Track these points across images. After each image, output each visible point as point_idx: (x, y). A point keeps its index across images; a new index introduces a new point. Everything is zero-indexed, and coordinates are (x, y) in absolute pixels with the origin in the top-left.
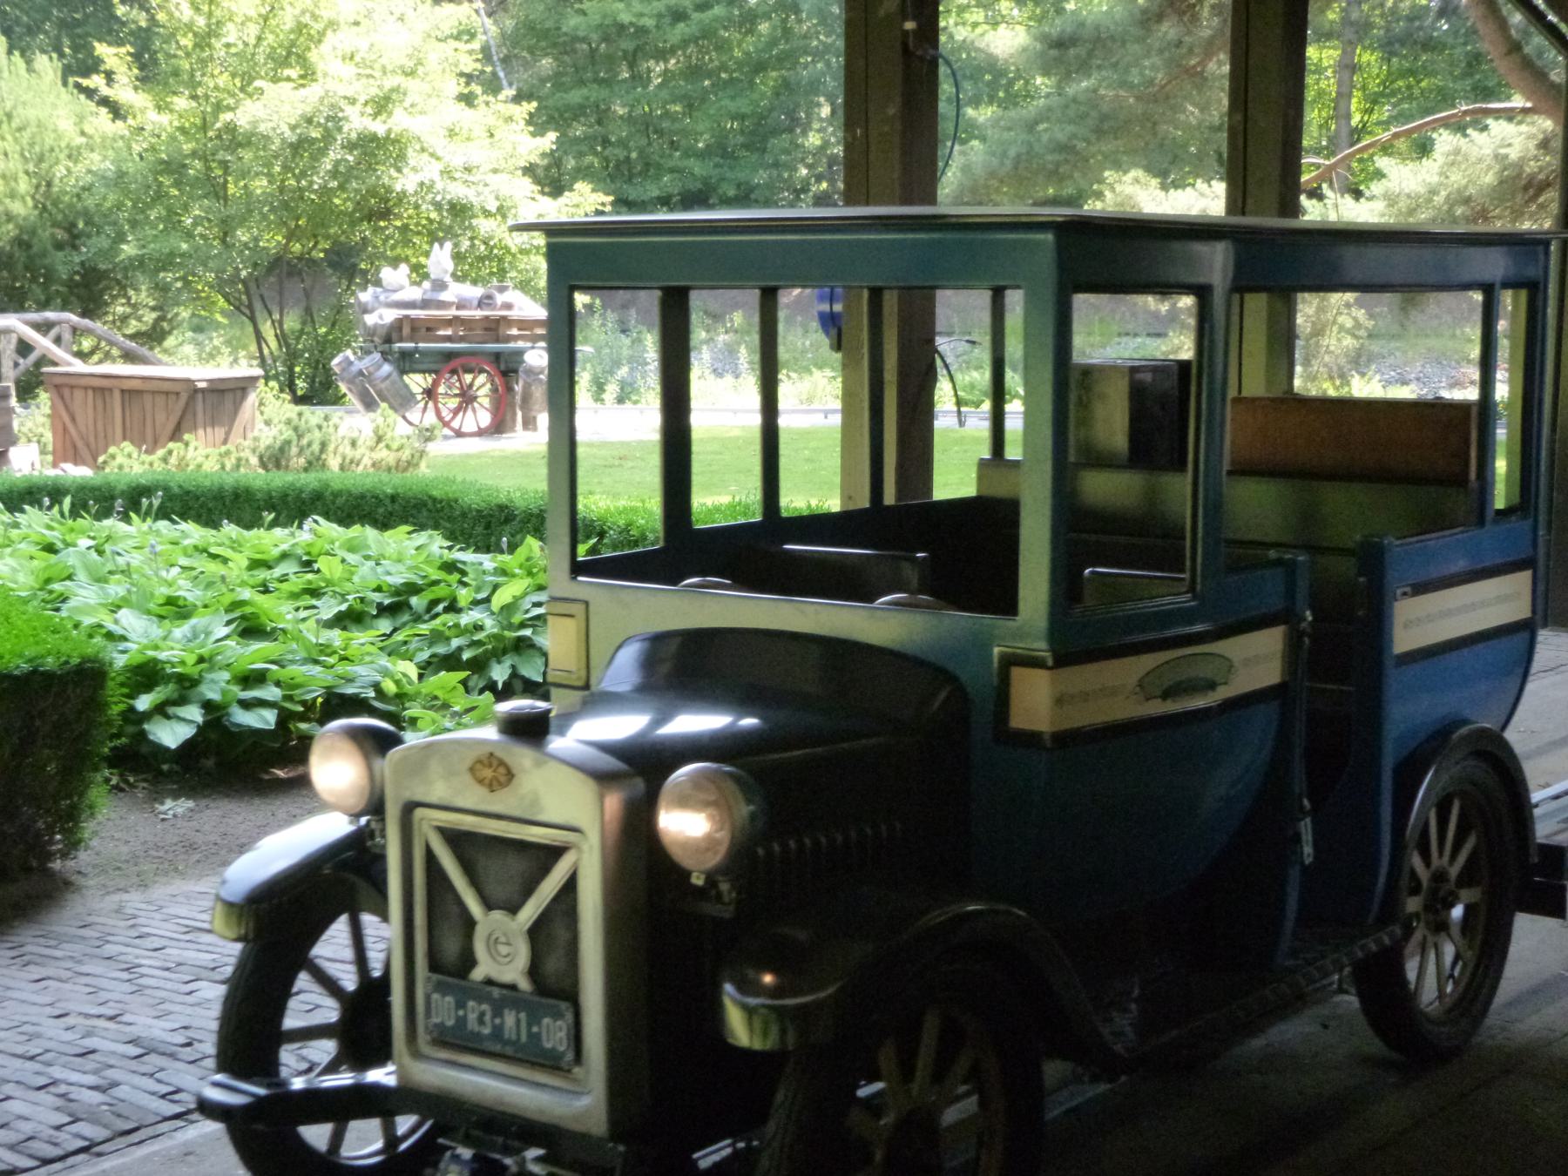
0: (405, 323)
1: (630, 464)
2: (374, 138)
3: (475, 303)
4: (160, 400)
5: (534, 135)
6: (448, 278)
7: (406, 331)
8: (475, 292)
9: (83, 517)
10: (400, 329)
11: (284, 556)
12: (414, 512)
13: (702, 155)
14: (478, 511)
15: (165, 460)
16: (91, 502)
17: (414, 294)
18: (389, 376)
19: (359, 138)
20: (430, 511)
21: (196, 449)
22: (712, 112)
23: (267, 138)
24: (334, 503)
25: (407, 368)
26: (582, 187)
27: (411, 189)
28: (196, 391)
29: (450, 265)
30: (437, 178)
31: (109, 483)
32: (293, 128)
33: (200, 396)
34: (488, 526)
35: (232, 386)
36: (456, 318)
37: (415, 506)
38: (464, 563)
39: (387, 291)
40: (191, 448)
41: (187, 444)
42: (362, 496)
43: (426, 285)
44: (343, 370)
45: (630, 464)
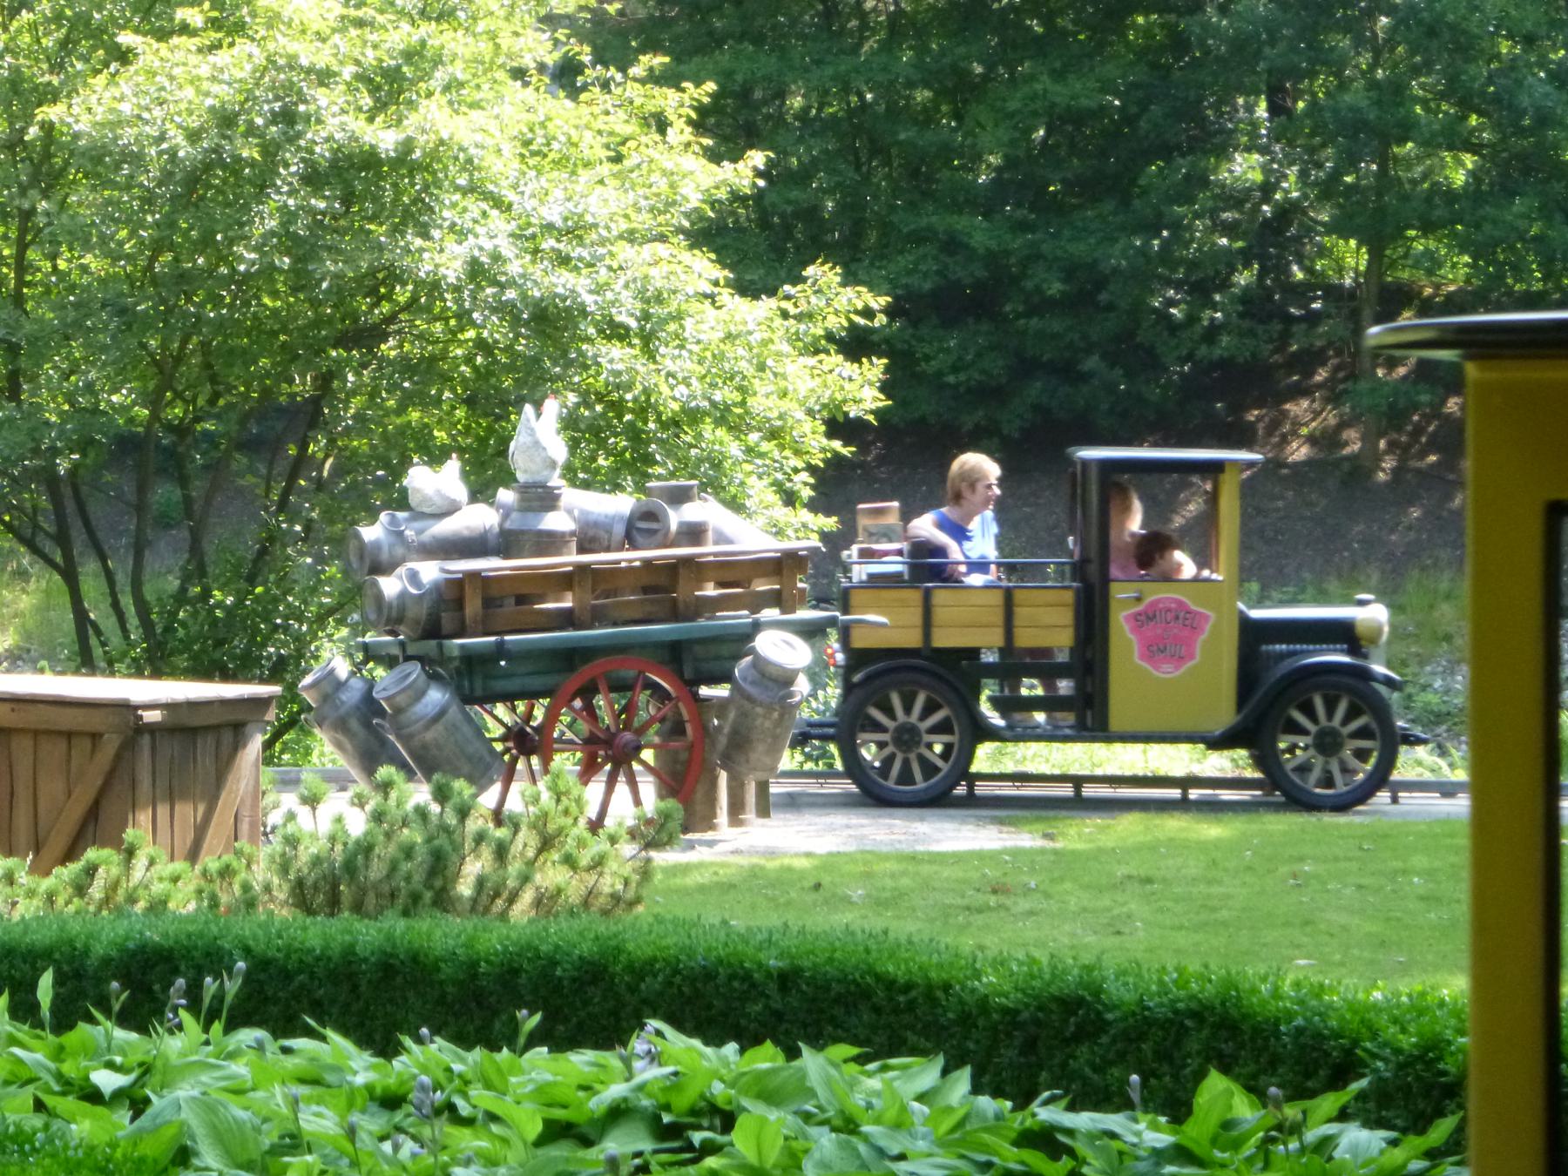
0: (468, 590)
1: (1024, 904)
2: (370, 161)
3: (619, 530)
4: (53, 751)
5: (714, 157)
6: (556, 481)
7: (473, 607)
8: (619, 505)
9: (91, 1020)
10: (459, 603)
11: (618, 1113)
12: (838, 1011)
13: (988, 203)
14: (1005, 1011)
15: (80, 890)
16: (115, 985)
17: (479, 518)
18: (442, 713)
19: (334, 163)
20: (877, 1010)
21: (152, 863)
22: (1013, 105)
23: (136, 159)
24: (633, 989)
25: (479, 692)
26: (822, 273)
27: (453, 271)
28: (142, 729)
29: (558, 449)
30: (507, 250)
31: (71, 942)
32: (193, 136)
33: (146, 740)
34: (1030, 1046)
35: (213, 720)
36: (582, 569)
37: (838, 1000)
38: (1070, 1132)
39: (420, 516)
40: (140, 862)
41: (130, 853)
42: (708, 975)
43: (506, 496)
44: (325, 698)
45: (1024, 904)
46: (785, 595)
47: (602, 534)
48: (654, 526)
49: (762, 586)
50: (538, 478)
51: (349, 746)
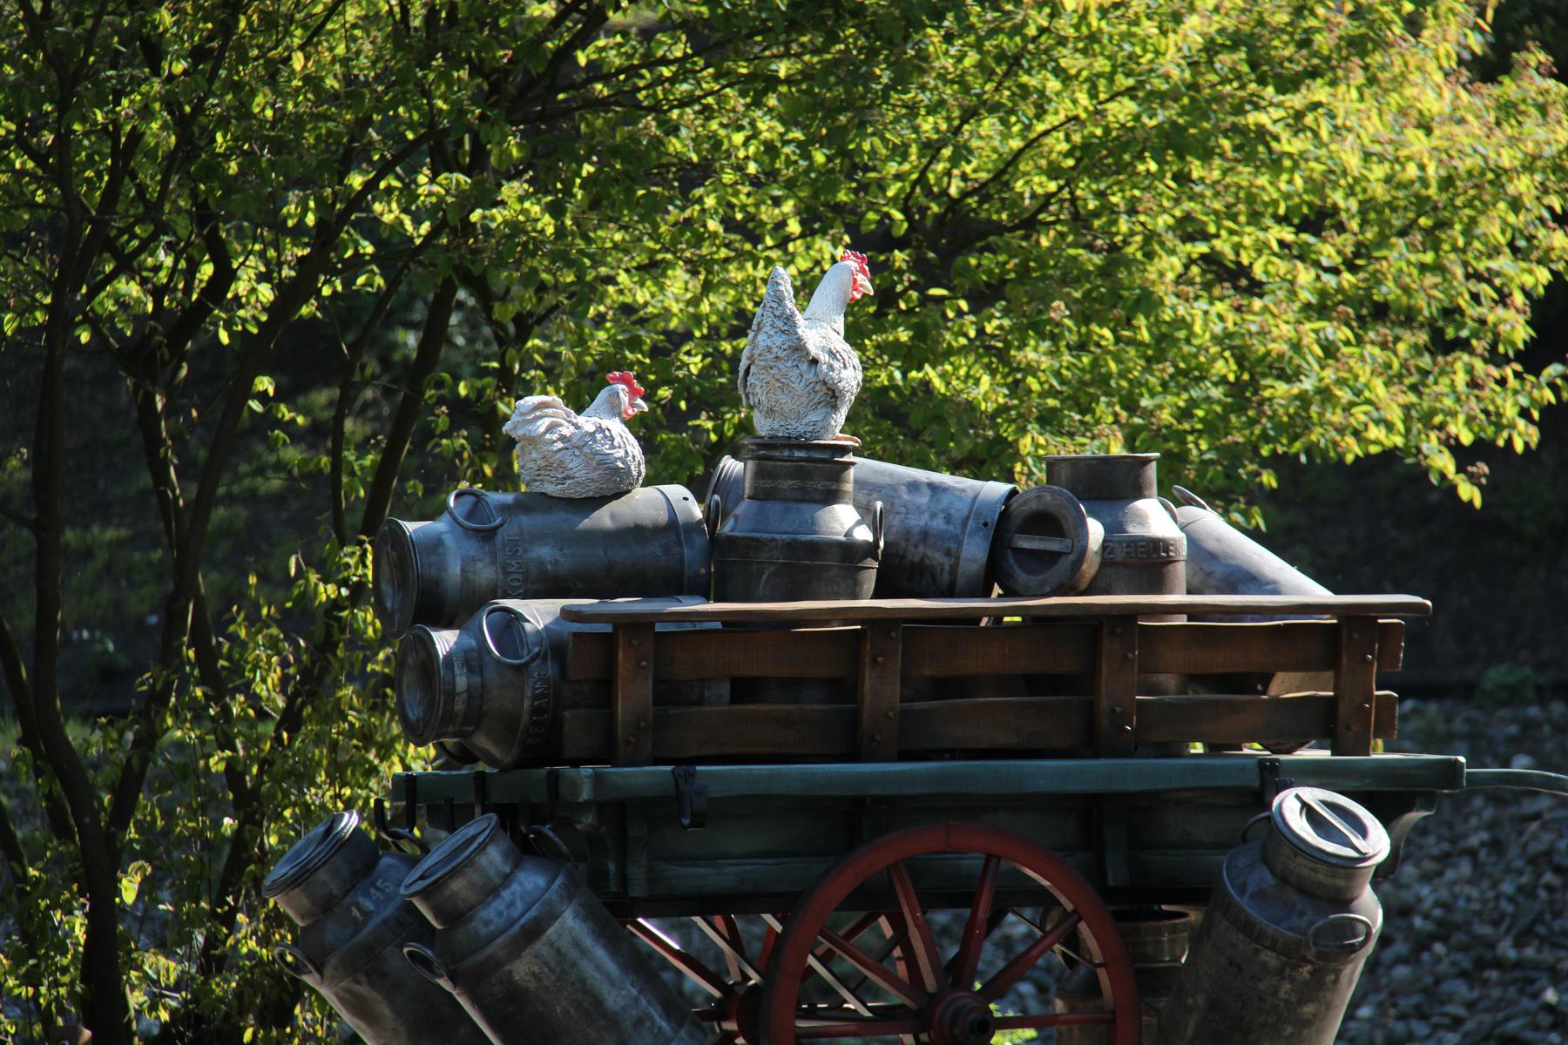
3: (974, 552)
46: (1344, 708)
47: (937, 557)
48: (1054, 545)
49: (1287, 687)
50: (798, 427)
51: (385, 1010)
